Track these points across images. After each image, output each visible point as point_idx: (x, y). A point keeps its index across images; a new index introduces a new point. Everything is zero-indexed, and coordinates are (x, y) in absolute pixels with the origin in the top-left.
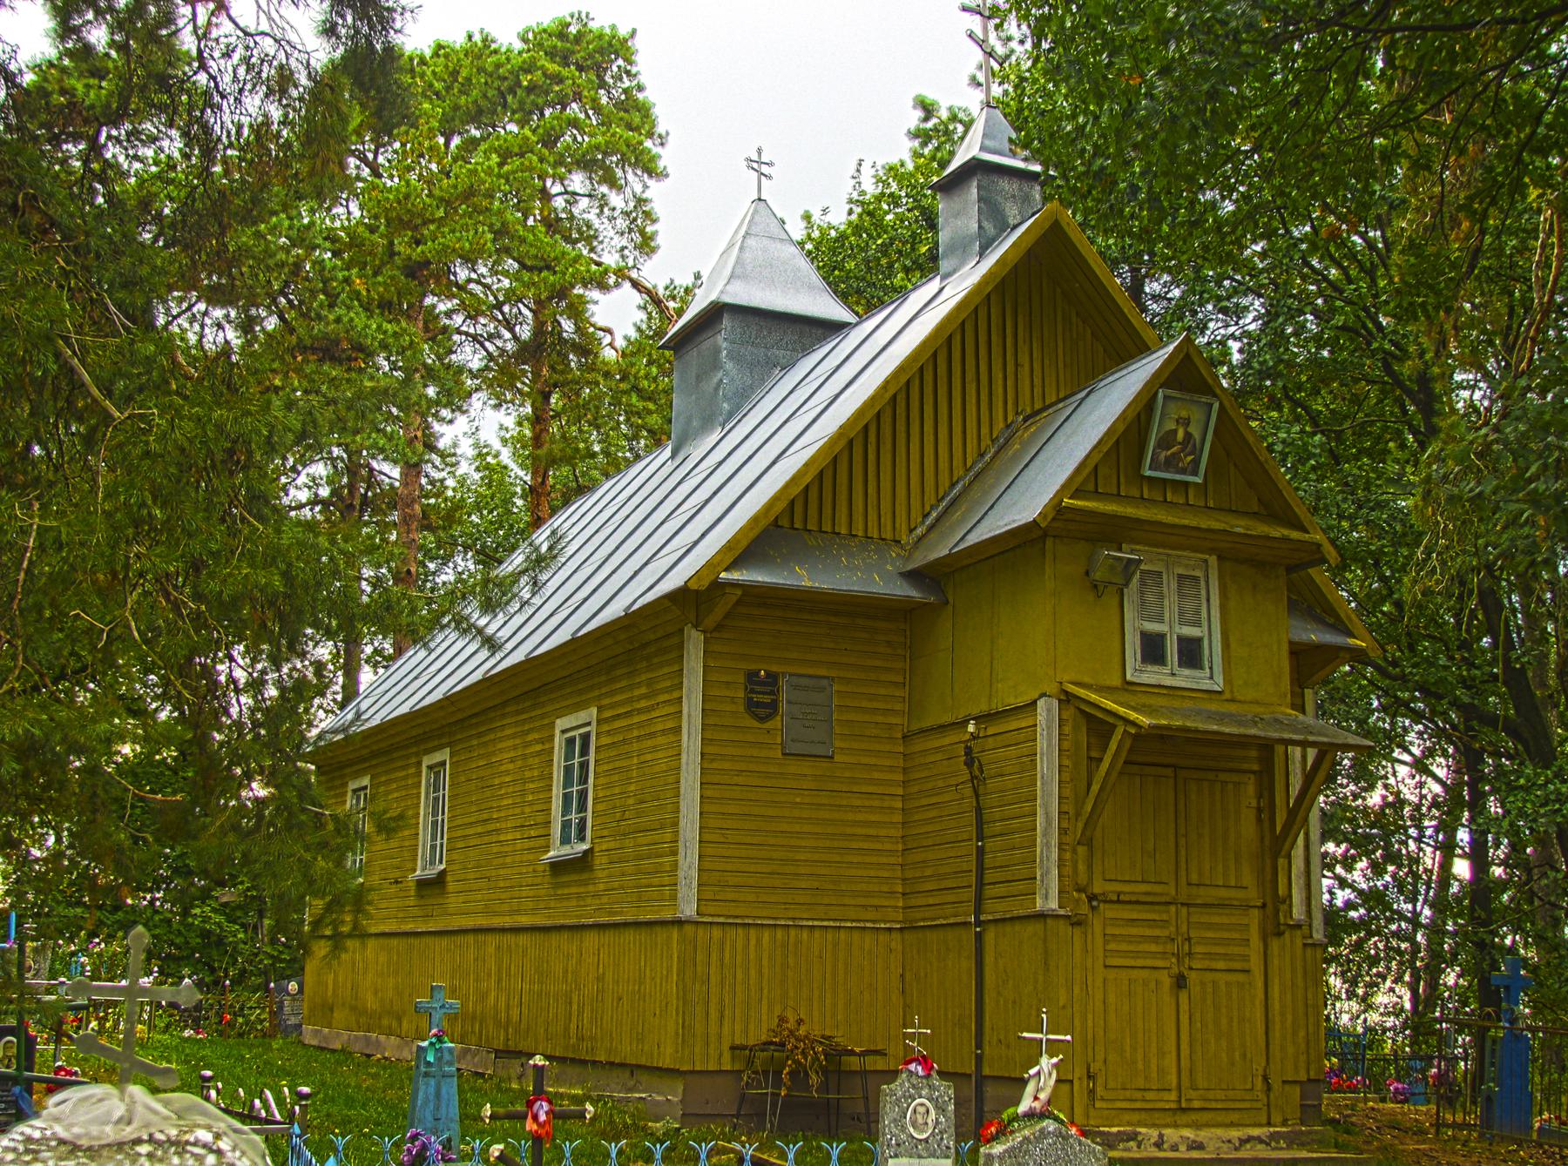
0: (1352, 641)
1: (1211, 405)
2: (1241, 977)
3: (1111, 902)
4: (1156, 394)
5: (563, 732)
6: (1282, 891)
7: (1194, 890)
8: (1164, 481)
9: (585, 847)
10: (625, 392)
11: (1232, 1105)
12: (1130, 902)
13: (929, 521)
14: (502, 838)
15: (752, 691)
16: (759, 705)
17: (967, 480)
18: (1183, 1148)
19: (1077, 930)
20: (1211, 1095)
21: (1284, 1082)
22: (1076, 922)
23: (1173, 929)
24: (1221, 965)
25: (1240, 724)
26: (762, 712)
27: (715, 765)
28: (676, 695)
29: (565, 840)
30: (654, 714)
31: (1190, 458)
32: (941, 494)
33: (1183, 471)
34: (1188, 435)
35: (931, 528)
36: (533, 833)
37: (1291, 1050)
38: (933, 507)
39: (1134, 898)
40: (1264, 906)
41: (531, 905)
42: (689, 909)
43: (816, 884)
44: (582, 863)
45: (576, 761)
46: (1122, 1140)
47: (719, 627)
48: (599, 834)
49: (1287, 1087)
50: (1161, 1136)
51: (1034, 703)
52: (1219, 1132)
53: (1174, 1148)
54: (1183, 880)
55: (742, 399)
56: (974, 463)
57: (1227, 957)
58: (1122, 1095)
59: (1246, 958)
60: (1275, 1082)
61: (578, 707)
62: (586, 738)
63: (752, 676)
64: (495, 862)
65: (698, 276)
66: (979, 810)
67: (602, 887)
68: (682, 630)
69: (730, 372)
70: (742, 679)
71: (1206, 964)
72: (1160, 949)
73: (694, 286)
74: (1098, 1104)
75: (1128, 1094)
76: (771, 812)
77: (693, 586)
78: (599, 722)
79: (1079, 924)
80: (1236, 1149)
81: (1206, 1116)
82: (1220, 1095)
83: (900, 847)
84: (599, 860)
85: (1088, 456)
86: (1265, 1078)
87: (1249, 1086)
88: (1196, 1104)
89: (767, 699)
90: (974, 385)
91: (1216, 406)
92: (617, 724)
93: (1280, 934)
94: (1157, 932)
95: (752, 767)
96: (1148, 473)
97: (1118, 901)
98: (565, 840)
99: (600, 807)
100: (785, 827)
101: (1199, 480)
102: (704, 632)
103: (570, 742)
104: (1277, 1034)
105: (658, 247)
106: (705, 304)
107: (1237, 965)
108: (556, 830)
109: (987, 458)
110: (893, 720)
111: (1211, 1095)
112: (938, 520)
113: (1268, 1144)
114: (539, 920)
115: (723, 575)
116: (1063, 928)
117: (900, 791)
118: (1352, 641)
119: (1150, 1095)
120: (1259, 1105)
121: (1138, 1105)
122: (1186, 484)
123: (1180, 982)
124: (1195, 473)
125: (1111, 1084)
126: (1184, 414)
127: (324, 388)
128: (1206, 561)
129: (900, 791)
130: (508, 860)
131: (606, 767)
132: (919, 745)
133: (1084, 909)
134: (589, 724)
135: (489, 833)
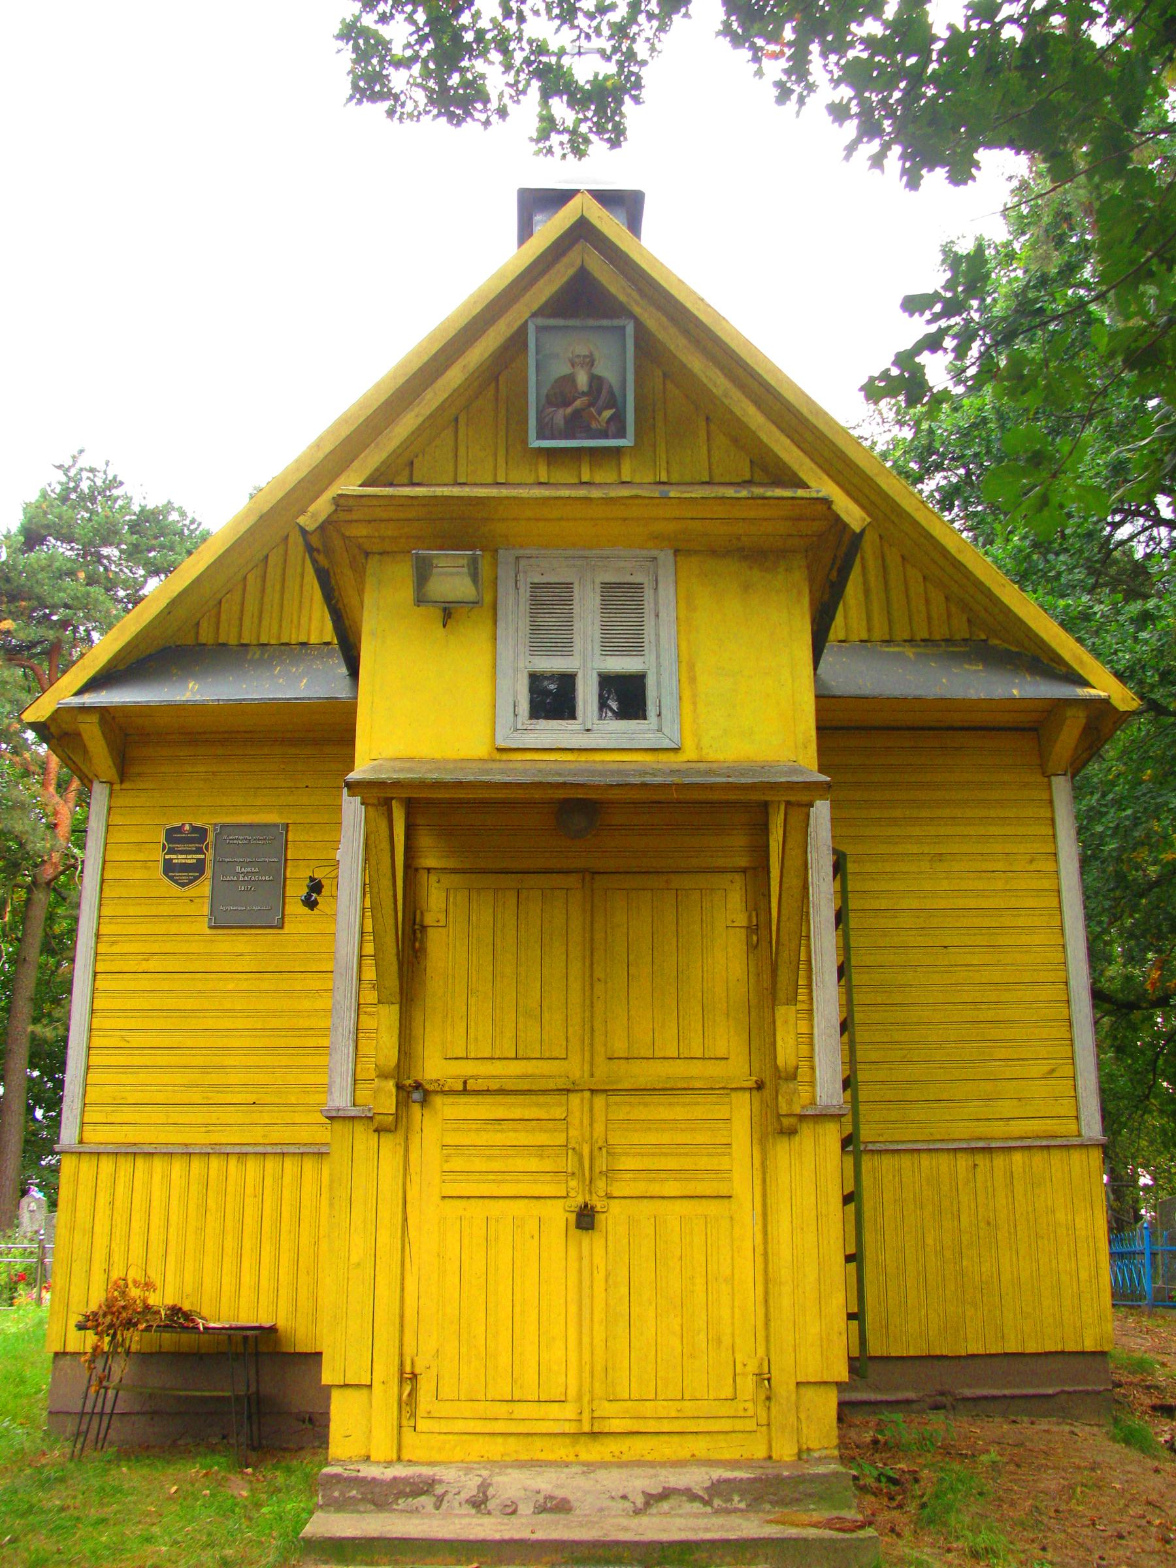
0: (1093, 692)
1: (623, 328)
2: (713, 1208)
7: (622, 1067)
11: (692, 1426)
12: (488, 1092)
15: (172, 851)
16: (185, 867)
18: (525, 1509)
20: (648, 1408)
21: (798, 1383)
24: (671, 1189)
25: (560, 775)
26: (184, 876)
27: (116, 949)
31: (607, 414)
37: (813, 1329)
39: (494, 1085)
40: (760, 1086)
43: (252, 1098)
46: (401, 1494)
49: (809, 1393)
53: (511, 1510)
54: (599, 1048)
57: (678, 1174)
58: (467, 1409)
59: (722, 1175)
60: (784, 1388)
63: (173, 835)
70: (162, 839)
71: (640, 1188)
72: (548, 1165)
74: (422, 1425)
75: (481, 1408)
76: (191, 1004)
80: (637, 1512)
82: (662, 1408)
87: (728, 1392)
88: (616, 1425)
89: (191, 859)
91: (630, 329)
93: (791, 1132)
94: (542, 1138)
95: (169, 947)
97: (465, 1091)
100: (211, 1023)
104: (786, 1302)
111: (648, 1408)
113: (706, 1503)
118: (1093, 692)
119: (521, 1410)
120: (750, 1425)
123: (586, 1219)
124: (621, 434)
125: (447, 1391)
127: (1099, 829)
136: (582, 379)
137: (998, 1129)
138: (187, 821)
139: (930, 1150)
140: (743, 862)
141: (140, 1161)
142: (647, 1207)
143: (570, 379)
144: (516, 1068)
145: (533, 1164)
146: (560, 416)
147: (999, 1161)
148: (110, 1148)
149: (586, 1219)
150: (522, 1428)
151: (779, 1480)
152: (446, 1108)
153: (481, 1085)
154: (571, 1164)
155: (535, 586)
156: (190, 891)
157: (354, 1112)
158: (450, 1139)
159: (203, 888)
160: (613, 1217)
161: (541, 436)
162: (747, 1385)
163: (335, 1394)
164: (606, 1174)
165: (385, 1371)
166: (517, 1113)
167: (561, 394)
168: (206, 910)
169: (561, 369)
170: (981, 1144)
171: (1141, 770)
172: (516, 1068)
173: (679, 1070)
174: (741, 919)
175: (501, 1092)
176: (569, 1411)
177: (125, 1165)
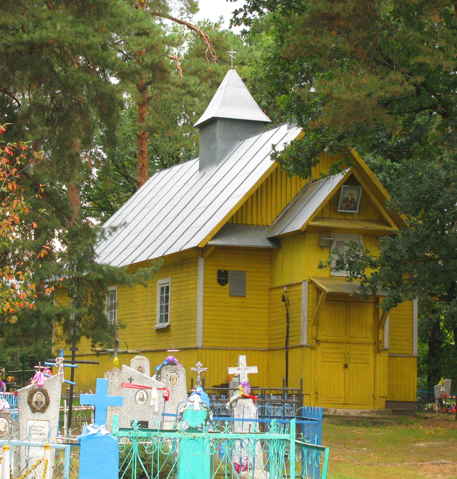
2: (366, 365)
3: (324, 342)
4: (341, 187)
5: (160, 285)
6: (380, 339)
8: (346, 213)
9: (167, 324)
10: (184, 95)
13: (278, 219)
14: (139, 320)
17: (292, 204)
19: (313, 351)
21: (380, 397)
22: (312, 348)
23: (344, 350)
24: (360, 361)
28: (196, 277)
29: (161, 321)
30: (189, 283)
31: (353, 205)
32: (283, 209)
33: (351, 209)
34: (353, 199)
35: (279, 221)
36: (150, 319)
38: (280, 214)
39: (331, 341)
40: (375, 344)
41: (150, 344)
42: (200, 344)
44: (166, 330)
45: (164, 295)
47: (209, 256)
48: (172, 320)
49: (381, 399)
50: (335, 410)
51: (301, 283)
52: (354, 410)
55: (225, 153)
56: (294, 198)
60: (377, 397)
61: (165, 277)
62: (167, 288)
64: (136, 328)
65: (221, 18)
66: (287, 315)
67: (174, 337)
68: (197, 257)
69: (220, 144)
72: (339, 356)
73: (220, 22)
74: (318, 401)
77: (200, 246)
78: (171, 283)
79: (313, 349)
81: (353, 406)
83: (267, 325)
84: (172, 329)
85: (317, 209)
86: (374, 396)
87: (368, 398)
88: (350, 403)
90: (280, 191)
91: (361, 189)
92: (178, 284)
93: (380, 352)
94: (339, 351)
96: (339, 211)
97: (326, 342)
98: (161, 321)
99: (172, 311)
101: (356, 212)
102: (204, 258)
103: (162, 288)
105: (198, 10)
106: (210, 117)
107: (365, 361)
108: (158, 318)
109: (299, 196)
110: (265, 284)
112: (281, 218)
114: (153, 348)
115: (209, 243)
116: (309, 350)
117: (268, 307)
119: (335, 399)
120: (371, 404)
121: (331, 402)
122: (353, 213)
123: (346, 366)
124: (355, 210)
126: (351, 192)
128: (359, 237)
129: (268, 307)
130: (141, 327)
131: (174, 298)
132: (273, 293)
133: (314, 344)
134: (168, 283)
135: (134, 318)
136: (350, 198)
137: (396, 352)
138: (223, 269)
139: (405, 356)
140: (373, 301)
141: (216, 351)
142: (355, 365)
143: (348, 198)
144: (335, 338)
145: (337, 356)
146: (344, 205)
147: (395, 358)
148: (210, 348)
149: (346, 366)
150: (335, 402)
151: (381, 411)
152: (323, 345)
153: (329, 341)
154: (343, 356)
155: (337, 241)
156: (225, 287)
157: (308, 345)
158: (323, 351)
159: (227, 286)
160: (350, 365)
161: (340, 209)
162: (371, 396)
163: (304, 396)
164: (349, 358)
165: (313, 392)
166: (334, 346)
167: (346, 200)
168: (228, 291)
169: (346, 196)
170: (392, 355)
171: (306, 110)
172: (335, 338)
173: (361, 340)
174: (373, 312)
175: (332, 342)
176: (343, 400)
177: (213, 352)
